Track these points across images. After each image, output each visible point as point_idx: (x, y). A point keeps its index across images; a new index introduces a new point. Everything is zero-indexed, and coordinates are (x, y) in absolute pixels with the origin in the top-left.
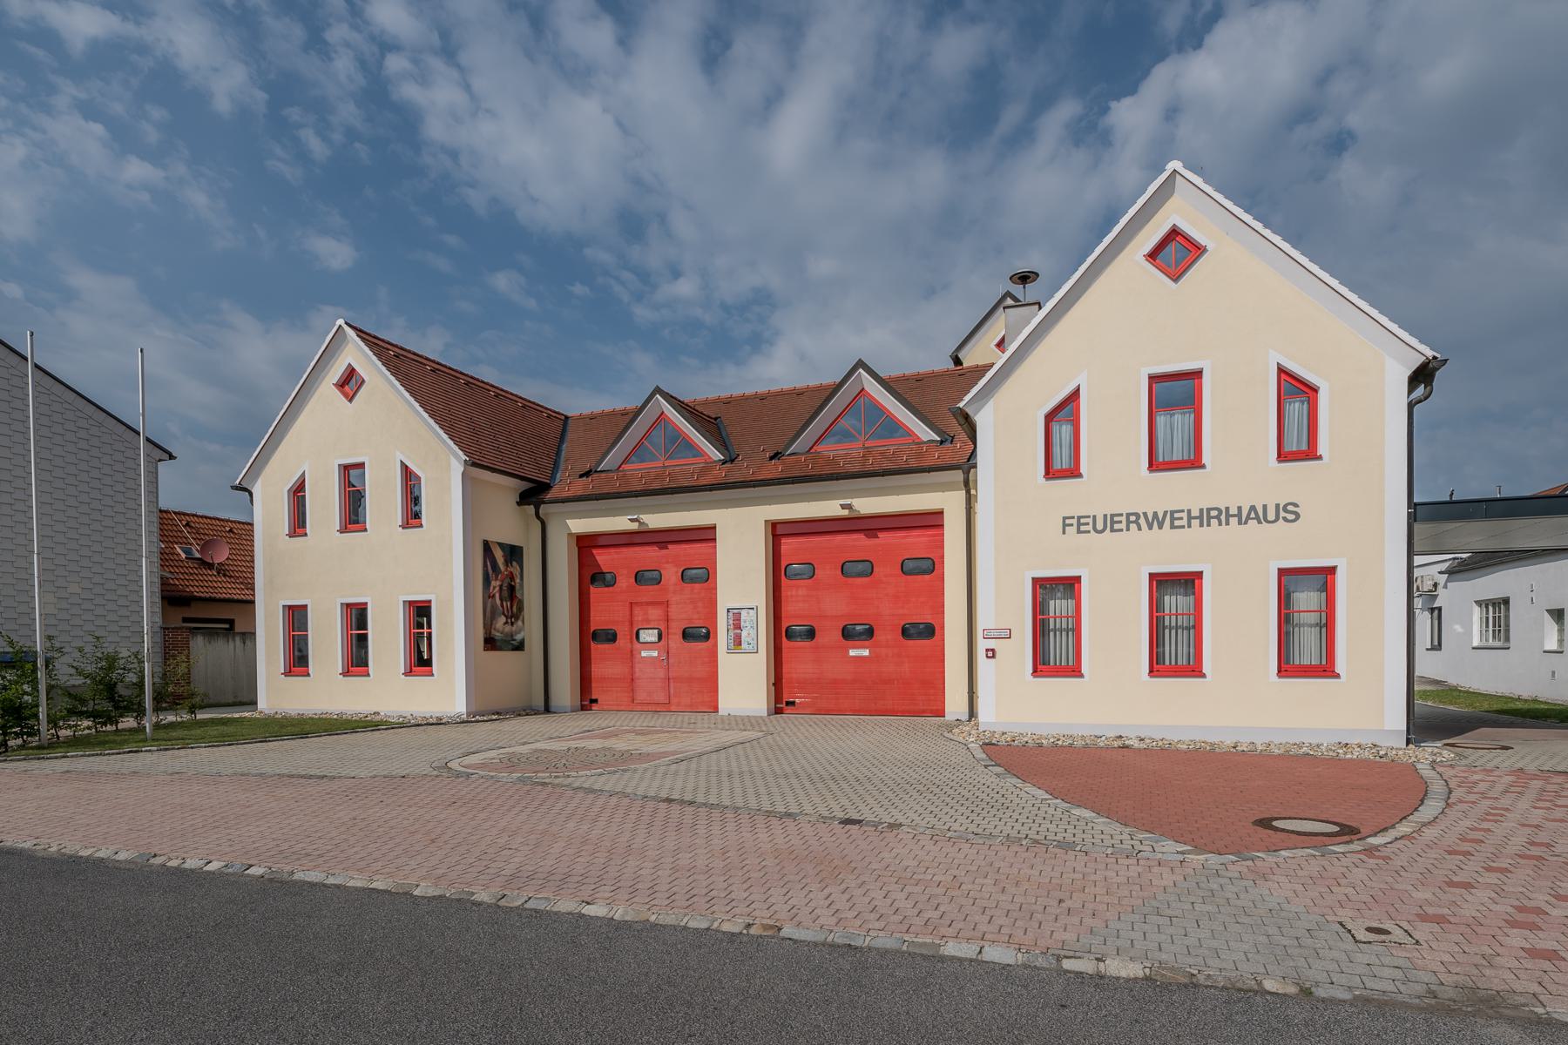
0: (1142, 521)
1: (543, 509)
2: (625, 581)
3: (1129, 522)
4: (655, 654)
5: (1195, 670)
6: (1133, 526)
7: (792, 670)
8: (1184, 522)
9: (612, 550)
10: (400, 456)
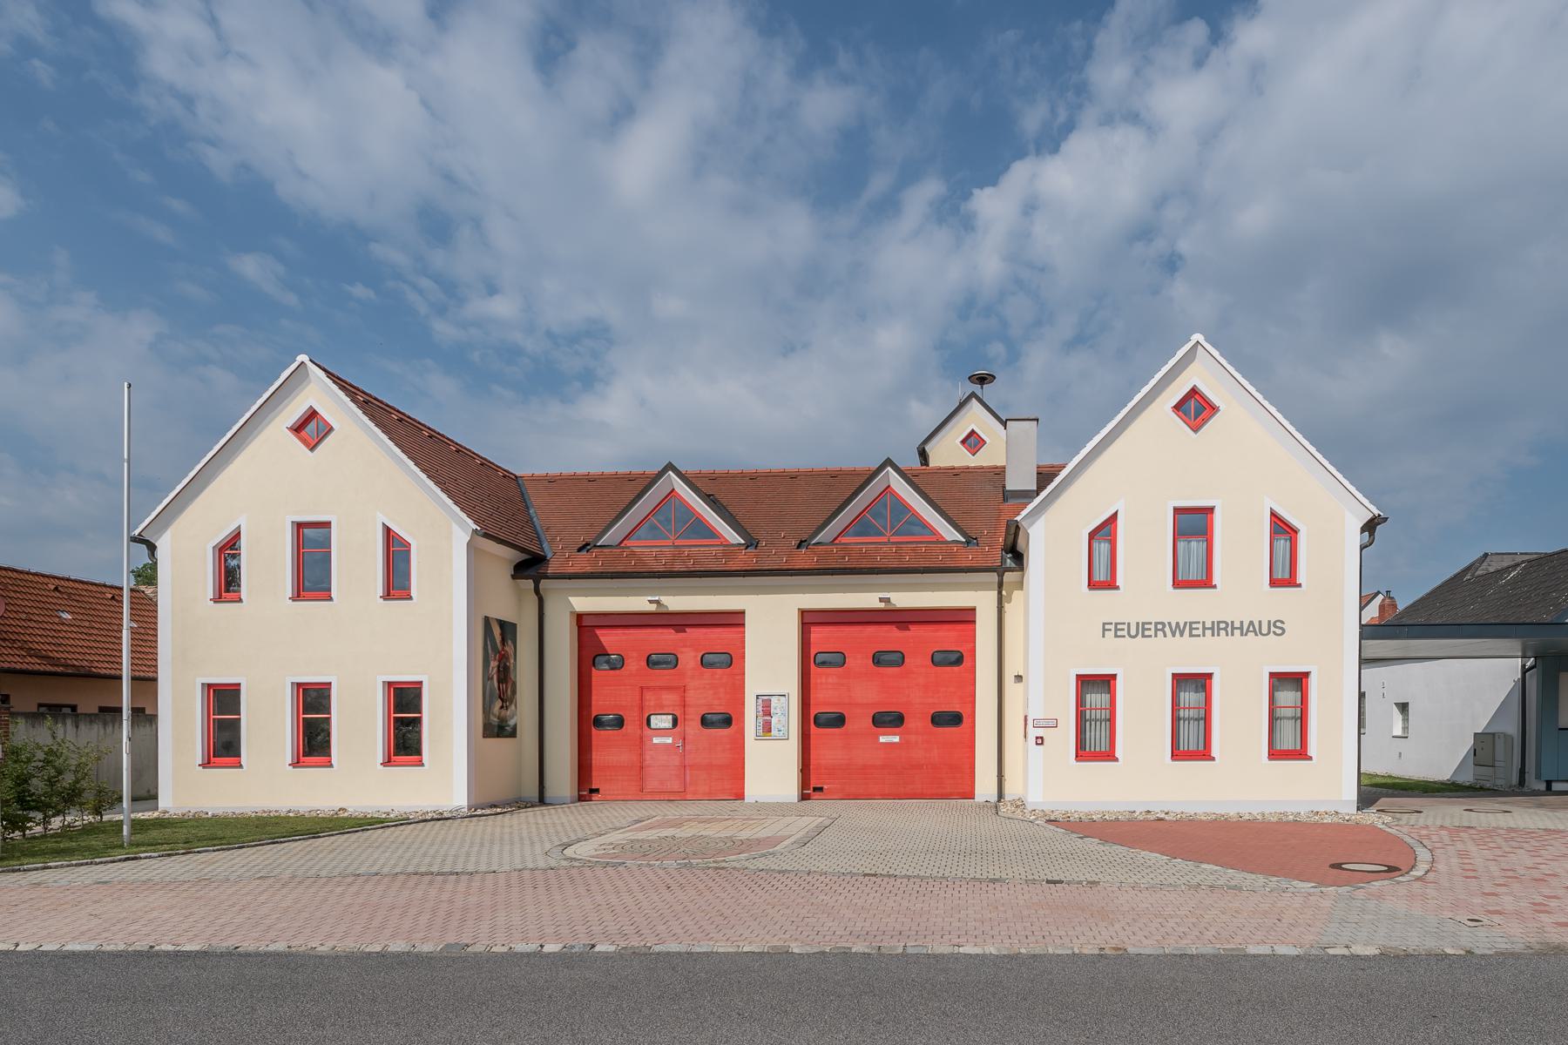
0: (1167, 629)
1: (544, 583)
2: (634, 665)
3: (1156, 630)
4: (669, 740)
5: (1110, 756)
6: (1160, 634)
7: (820, 756)
8: (1200, 632)
9: (619, 631)
10: (382, 518)
